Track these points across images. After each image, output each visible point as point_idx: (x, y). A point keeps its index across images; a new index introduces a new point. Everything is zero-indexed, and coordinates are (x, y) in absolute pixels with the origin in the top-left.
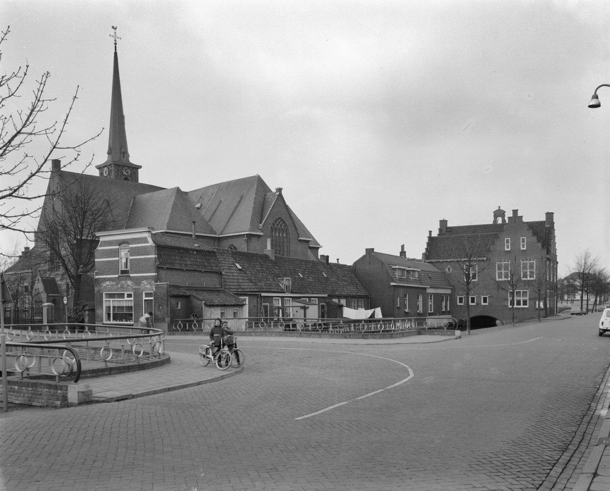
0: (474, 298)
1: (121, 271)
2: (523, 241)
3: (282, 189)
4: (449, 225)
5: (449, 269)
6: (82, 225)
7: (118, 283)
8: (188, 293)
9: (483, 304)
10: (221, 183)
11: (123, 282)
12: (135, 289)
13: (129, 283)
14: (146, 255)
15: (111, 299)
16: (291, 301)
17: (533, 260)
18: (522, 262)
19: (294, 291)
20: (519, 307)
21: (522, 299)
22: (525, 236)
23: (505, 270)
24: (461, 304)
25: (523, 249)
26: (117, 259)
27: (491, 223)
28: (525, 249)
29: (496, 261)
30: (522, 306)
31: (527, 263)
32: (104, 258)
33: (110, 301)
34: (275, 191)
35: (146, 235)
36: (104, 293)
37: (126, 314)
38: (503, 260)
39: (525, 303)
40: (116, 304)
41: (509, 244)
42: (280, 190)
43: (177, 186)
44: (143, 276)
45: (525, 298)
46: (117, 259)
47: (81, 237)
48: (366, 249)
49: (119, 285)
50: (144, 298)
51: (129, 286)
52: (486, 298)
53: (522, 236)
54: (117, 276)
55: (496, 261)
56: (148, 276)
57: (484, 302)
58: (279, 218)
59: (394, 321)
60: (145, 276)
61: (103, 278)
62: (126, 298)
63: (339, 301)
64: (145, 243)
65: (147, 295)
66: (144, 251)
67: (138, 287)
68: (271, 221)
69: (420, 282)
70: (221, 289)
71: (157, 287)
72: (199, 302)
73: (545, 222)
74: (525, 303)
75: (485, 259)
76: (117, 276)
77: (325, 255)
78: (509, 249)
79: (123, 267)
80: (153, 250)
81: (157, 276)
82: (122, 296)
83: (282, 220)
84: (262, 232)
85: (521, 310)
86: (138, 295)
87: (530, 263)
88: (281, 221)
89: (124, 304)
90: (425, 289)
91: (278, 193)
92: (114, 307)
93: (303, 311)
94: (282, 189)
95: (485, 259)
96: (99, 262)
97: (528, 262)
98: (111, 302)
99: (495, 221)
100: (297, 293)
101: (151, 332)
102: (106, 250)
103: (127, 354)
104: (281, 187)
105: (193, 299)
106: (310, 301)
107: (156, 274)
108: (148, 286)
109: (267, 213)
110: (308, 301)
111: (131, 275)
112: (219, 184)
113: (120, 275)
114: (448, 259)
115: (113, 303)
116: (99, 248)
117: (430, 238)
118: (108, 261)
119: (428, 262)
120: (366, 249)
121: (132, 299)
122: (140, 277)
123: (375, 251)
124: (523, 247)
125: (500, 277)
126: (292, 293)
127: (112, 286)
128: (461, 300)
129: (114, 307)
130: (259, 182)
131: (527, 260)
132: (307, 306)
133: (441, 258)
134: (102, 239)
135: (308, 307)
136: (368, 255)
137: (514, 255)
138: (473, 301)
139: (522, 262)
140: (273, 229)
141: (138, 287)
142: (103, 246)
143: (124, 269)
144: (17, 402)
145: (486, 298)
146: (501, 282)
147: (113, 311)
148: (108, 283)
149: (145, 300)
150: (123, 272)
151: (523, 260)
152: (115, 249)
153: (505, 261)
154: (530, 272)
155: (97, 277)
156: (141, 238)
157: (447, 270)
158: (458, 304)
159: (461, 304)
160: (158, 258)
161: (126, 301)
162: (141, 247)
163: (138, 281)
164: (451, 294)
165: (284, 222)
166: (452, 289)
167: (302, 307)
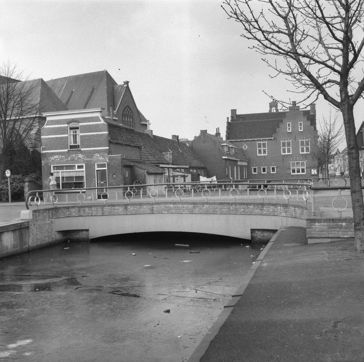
0: (265, 168)
1: (70, 146)
2: (301, 124)
3: (129, 82)
4: (238, 113)
5: (245, 147)
6: (6, 108)
7: (68, 157)
8: (132, 164)
9: (262, 173)
10: (69, 77)
11: (74, 156)
12: (87, 161)
13: (80, 156)
14: (98, 131)
15: (60, 171)
16: (172, 171)
17: (290, 140)
18: (300, 140)
19: (174, 163)
20: (294, 174)
21: (301, 168)
22: (302, 121)
23: (287, 146)
24: (255, 173)
25: (289, 131)
26: (67, 135)
27: (268, 112)
28: (302, 130)
29: (281, 140)
30: (301, 173)
31: (304, 141)
32: (52, 135)
33: (59, 172)
34: (123, 84)
35: (98, 115)
36: (52, 166)
37: (66, 183)
38: (286, 139)
39: (303, 171)
40: (65, 175)
41: (291, 127)
42: (127, 83)
43: (40, 77)
44: (95, 150)
45: (303, 167)
46: (67, 135)
47: (5, 118)
48: (201, 131)
49: (69, 158)
50: (97, 169)
51: (79, 158)
52: (256, 169)
53: (300, 121)
54: (66, 150)
55: (281, 140)
56: (100, 150)
57: (263, 172)
58: (128, 106)
59: (225, 185)
60: (98, 150)
61: (51, 153)
62: (77, 169)
63: (193, 171)
64: (96, 121)
65: (99, 166)
66: (96, 128)
67: (89, 159)
68: (122, 109)
69: (234, 156)
70: (141, 161)
71: (110, 159)
72: (142, 171)
73: (309, 111)
74: (303, 171)
75: (273, 138)
76: (66, 150)
77: (177, 135)
78: (290, 131)
79: (73, 142)
80: (106, 127)
81: (109, 149)
82: (72, 167)
83: (129, 107)
84: (116, 117)
85: (300, 176)
86: (89, 167)
87: (306, 141)
88: (128, 108)
89: (74, 175)
90: (237, 161)
91: (126, 85)
92: (63, 178)
93: (183, 179)
94: (129, 82)
95: (273, 138)
96: (46, 139)
97: (286, 141)
98: (60, 173)
99: (270, 110)
100: (175, 165)
101: (240, 186)
102: (54, 128)
103: (233, 206)
104: (126, 80)
105: (137, 169)
106: (180, 170)
107: (107, 148)
108: (101, 158)
109: (118, 103)
110: (179, 170)
111: (82, 149)
112: (67, 77)
113: (69, 149)
114: (244, 139)
115: (60, 174)
116: (46, 126)
117: (228, 123)
118: (56, 138)
119: (229, 142)
120: (201, 131)
121: (84, 169)
122: (92, 150)
123: (208, 132)
124: (289, 130)
125: (303, 151)
126: (173, 164)
127: (62, 159)
128: (255, 170)
129: (63, 178)
130: (106, 76)
131: (303, 139)
132: (186, 175)
133: (239, 138)
134: (48, 119)
135: (188, 176)
136: (202, 136)
137: (294, 135)
138: (264, 170)
139: (300, 140)
140: (123, 115)
141: (89, 159)
142: (50, 125)
143: (73, 144)
144: (347, 237)
145: (256, 169)
146: (285, 155)
147: (62, 181)
148: (56, 157)
149: (97, 170)
150: (71, 147)
151: (301, 139)
152: (64, 127)
153: (287, 140)
154: (288, 149)
155: (44, 152)
156: (92, 117)
157: (244, 147)
158: (253, 173)
159: (255, 173)
160: (109, 134)
161: (77, 171)
162: (93, 125)
163: (90, 154)
164: (248, 166)
165: (130, 109)
166: (248, 162)
167: (182, 176)
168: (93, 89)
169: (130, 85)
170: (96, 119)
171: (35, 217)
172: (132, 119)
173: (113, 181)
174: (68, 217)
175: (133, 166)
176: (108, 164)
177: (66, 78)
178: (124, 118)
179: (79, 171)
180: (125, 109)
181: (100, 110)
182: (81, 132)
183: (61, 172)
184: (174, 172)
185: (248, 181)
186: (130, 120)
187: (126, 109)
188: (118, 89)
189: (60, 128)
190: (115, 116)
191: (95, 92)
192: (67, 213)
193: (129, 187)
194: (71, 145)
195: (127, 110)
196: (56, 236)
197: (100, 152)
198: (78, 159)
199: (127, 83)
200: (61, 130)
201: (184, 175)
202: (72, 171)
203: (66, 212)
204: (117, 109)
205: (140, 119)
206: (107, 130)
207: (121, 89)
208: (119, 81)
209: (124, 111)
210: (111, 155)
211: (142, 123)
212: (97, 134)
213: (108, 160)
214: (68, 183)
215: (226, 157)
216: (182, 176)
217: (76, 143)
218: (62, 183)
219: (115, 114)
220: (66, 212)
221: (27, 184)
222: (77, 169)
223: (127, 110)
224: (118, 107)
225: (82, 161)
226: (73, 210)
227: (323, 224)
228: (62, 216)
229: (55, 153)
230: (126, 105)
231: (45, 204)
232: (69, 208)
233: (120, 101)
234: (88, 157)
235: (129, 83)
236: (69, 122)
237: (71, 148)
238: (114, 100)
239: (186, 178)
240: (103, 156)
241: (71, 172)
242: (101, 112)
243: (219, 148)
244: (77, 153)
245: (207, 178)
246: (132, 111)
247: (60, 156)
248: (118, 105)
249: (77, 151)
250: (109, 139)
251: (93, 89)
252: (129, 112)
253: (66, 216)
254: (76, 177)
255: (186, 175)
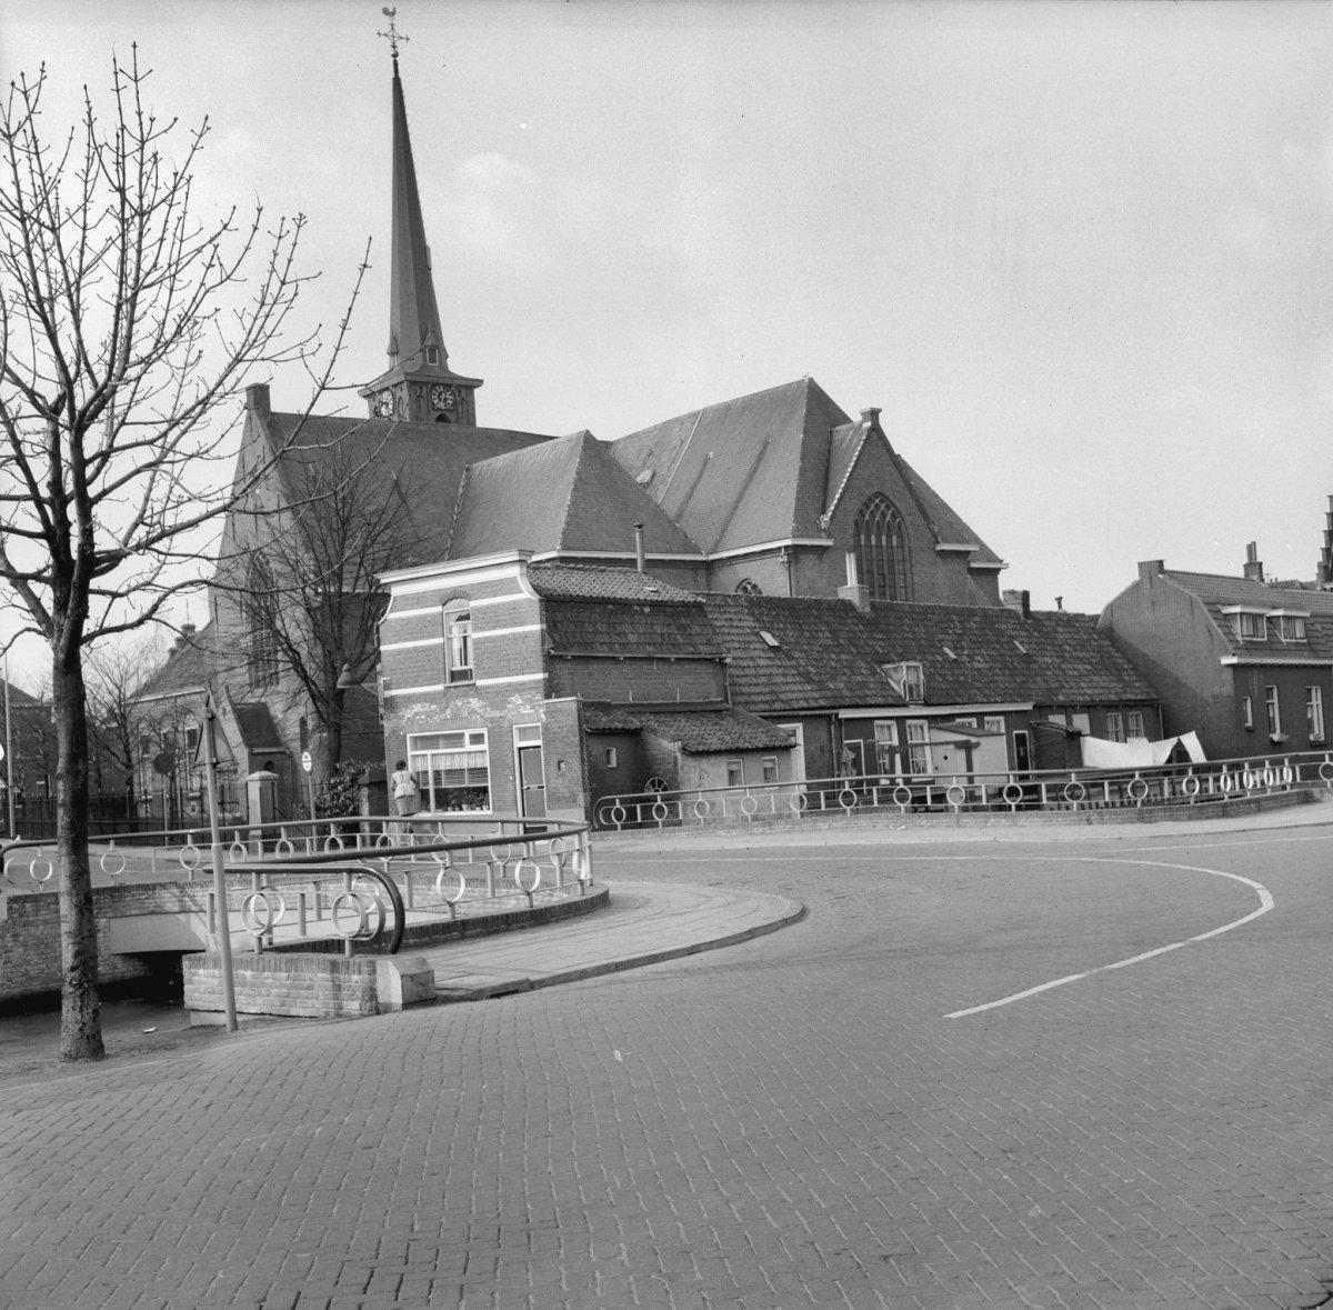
3: (880, 410)
8: (635, 723)
11: (459, 704)
12: (492, 720)
13: (475, 703)
40: (444, 765)
43: (582, 428)
44: (509, 685)
49: (449, 711)
50: (519, 744)
51: (473, 712)
54: (440, 687)
56: (523, 684)
58: (878, 494)
62: (468, 747)
64: (511, 592)
66: (511, 615)
68: (854, 505)
76: (440, 687)
77: (1019, 588)
80: (536, 609)
82: (456, 739)
83: (885, 498)
88: (882, 501)
89: (464, 763)
92: (437, 773)
94: (880, 410)
102: (409, 620)
105: (650, 738)
106: (981, 724)
108: (527, 710)
109: (838, 487)
110: (975, 725)
111: (480, 683)
120: (1140, 565)
121: (485, 747)
126: (927, 704)
127: (429, 715)
136: (1147, 585)
143: (458, 667)
148: (417, 708)
149: (520, 749)
150: (455, 676)
152: (433, 616)
161: (469, 753)
163: (497, 697)
165: (890, 504)
167: (959, 745)
168: (766, 444)
169: (885, 423)
170: (507, 586)
171: (21, 916)
172: (900, 537)
173: (560, 781)
174: (153, 913)
175: (641, 729)
176: (546, 728)
177: (695, 415)
178: (862, 537)
179: (476, 752)
180: (866, 505)
181: (517, 558)
182: (475, 629)
183: (433, 755)
184: (934, 732)
185: (112, 842)
186: (868, 539)
187: (872, 505)
188: (844, 439)
189: (423, 618)
190: (823, 534)
191: (768, 453)
192: (150, 903)
193: (282, 829)
194: (454, 669)
195: (877, 506)
196: (116, 967)
197: (524, 690)
198: (469, 713)
199: (874, 414)
200: (427, 623)
201: (968, 742)
202: (459, 753)
203: (147, 898)
204: (832, 508)
205: (935, 536)
206: (538, 617)
207: (852, 439)
208: (853, 409)
209: (861, 513)
210: (556, 697)
211: (939, 548)
212: (514, 634)
213: (543, 716)
214: (474, 789)
215: (1234, 660)
216: (959, 745)
217: (466, 664)
218: (437, 791)
219: (823, 525)
220: (147, 898)
221: (365, 792)
222: (468, 747)
223: (877, 506)
224: (835, 502)
225: (479, 721)
226: (165, 894)
227: (211, 971)
228: (134, 912)
229: (414, 695)
230: (875, 489)
231: (260, 859)
232: (154, 889)
233: (845, 480)
234: (494, 707)
235: (880, 415)
236: (447, 598)
237: (453, 680)
238: (827, 478)
239: (975, 753)
240: (530, 701)
241: (456, 756)
242: (520, 561)
243: (1207, 627)
244: (466, 695)
245: (1150, 741)
246: (896, 508)
247: (427, 705)
248: (838, 496)
249: (466, 688)
250: (547, 647)
251: (766, 444)
252: (883, 515)
253: (146, 911)
254: (472, 770)
255: (974, 740)
